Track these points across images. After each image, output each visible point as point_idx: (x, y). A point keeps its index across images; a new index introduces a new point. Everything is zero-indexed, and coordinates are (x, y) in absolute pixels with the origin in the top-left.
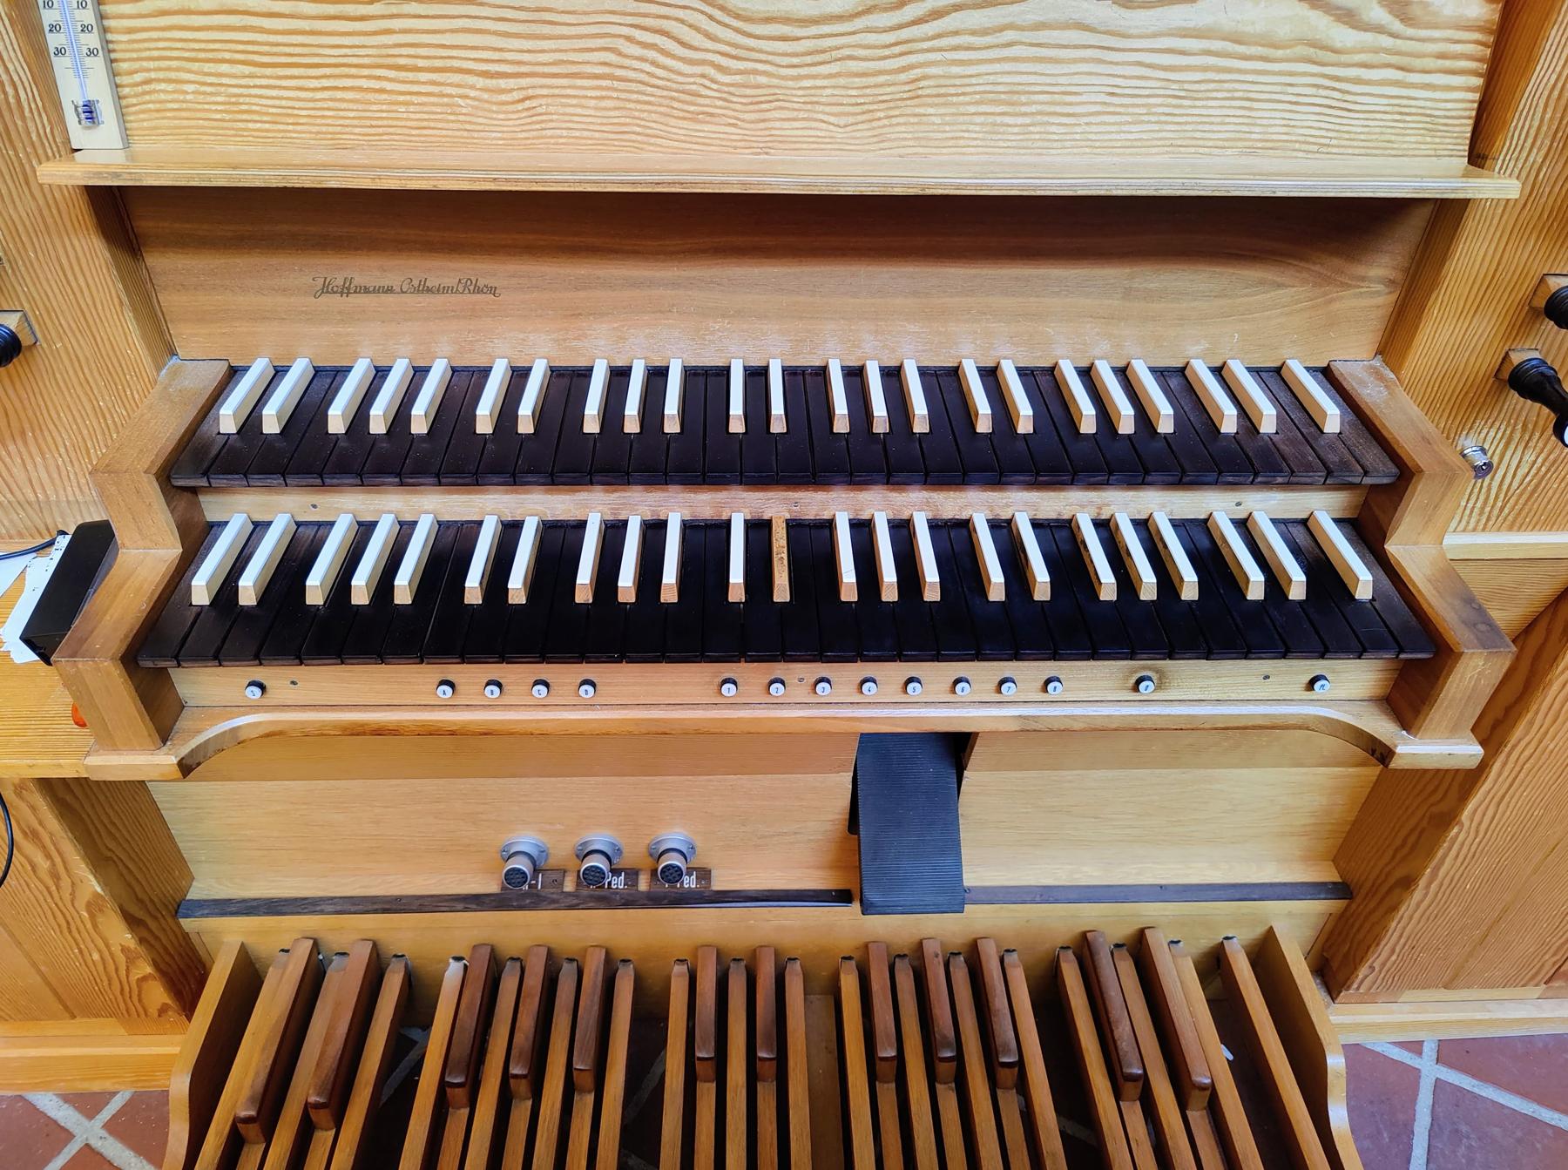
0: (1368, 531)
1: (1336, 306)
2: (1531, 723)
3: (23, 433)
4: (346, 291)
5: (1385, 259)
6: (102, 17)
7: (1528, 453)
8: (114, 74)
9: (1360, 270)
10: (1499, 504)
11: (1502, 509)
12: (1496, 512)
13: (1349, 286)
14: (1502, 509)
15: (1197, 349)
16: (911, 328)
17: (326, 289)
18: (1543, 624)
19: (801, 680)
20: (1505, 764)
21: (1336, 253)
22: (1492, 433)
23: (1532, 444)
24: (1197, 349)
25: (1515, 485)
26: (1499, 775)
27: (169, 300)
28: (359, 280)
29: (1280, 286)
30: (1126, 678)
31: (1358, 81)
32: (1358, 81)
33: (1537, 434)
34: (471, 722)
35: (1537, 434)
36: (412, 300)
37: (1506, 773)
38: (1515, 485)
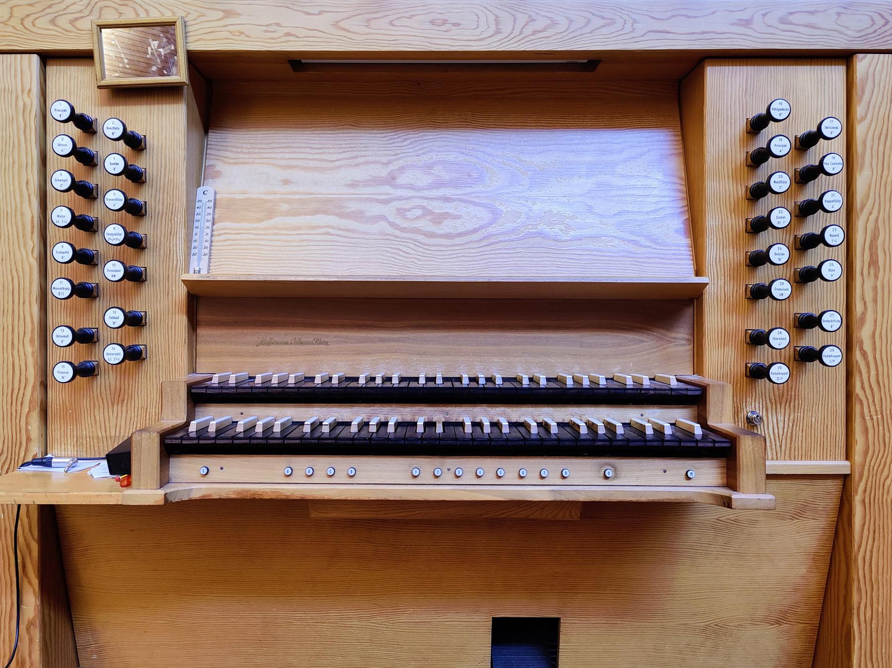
0: (702, 420)
1: (669, 350)
2: (859, 589)
3: (123, 401)
4: (269, 344)
5: (682, 330)
6: (211, 246)
7: (779, 415)
8: (210, 262)
9: (674, 335)
10: (778, 444)
11: (781, 447)
12: (778, 448)
13: (671, 342)
14: (781, 447)
15: (616, 369)
16: (496, 360)
17: (262, 343)
18: (840, 528)
19: (449, 470)
20: (859, 625)
21: (661, 327)
22: (757, 405)
23: (778, 410)
24: (616, 369)
25: (781, 433)
26: (860, 633)
27: (201, 348)
28: (276, 339)
29: (642, 341)
30: (599, 471)
31: (645, 263)
32: (645, 263)
33: (778, 406)
34: (297, 490)
35: (778, 406)
36: (294, 348)
37: (864, 632)
38: (781, 433)
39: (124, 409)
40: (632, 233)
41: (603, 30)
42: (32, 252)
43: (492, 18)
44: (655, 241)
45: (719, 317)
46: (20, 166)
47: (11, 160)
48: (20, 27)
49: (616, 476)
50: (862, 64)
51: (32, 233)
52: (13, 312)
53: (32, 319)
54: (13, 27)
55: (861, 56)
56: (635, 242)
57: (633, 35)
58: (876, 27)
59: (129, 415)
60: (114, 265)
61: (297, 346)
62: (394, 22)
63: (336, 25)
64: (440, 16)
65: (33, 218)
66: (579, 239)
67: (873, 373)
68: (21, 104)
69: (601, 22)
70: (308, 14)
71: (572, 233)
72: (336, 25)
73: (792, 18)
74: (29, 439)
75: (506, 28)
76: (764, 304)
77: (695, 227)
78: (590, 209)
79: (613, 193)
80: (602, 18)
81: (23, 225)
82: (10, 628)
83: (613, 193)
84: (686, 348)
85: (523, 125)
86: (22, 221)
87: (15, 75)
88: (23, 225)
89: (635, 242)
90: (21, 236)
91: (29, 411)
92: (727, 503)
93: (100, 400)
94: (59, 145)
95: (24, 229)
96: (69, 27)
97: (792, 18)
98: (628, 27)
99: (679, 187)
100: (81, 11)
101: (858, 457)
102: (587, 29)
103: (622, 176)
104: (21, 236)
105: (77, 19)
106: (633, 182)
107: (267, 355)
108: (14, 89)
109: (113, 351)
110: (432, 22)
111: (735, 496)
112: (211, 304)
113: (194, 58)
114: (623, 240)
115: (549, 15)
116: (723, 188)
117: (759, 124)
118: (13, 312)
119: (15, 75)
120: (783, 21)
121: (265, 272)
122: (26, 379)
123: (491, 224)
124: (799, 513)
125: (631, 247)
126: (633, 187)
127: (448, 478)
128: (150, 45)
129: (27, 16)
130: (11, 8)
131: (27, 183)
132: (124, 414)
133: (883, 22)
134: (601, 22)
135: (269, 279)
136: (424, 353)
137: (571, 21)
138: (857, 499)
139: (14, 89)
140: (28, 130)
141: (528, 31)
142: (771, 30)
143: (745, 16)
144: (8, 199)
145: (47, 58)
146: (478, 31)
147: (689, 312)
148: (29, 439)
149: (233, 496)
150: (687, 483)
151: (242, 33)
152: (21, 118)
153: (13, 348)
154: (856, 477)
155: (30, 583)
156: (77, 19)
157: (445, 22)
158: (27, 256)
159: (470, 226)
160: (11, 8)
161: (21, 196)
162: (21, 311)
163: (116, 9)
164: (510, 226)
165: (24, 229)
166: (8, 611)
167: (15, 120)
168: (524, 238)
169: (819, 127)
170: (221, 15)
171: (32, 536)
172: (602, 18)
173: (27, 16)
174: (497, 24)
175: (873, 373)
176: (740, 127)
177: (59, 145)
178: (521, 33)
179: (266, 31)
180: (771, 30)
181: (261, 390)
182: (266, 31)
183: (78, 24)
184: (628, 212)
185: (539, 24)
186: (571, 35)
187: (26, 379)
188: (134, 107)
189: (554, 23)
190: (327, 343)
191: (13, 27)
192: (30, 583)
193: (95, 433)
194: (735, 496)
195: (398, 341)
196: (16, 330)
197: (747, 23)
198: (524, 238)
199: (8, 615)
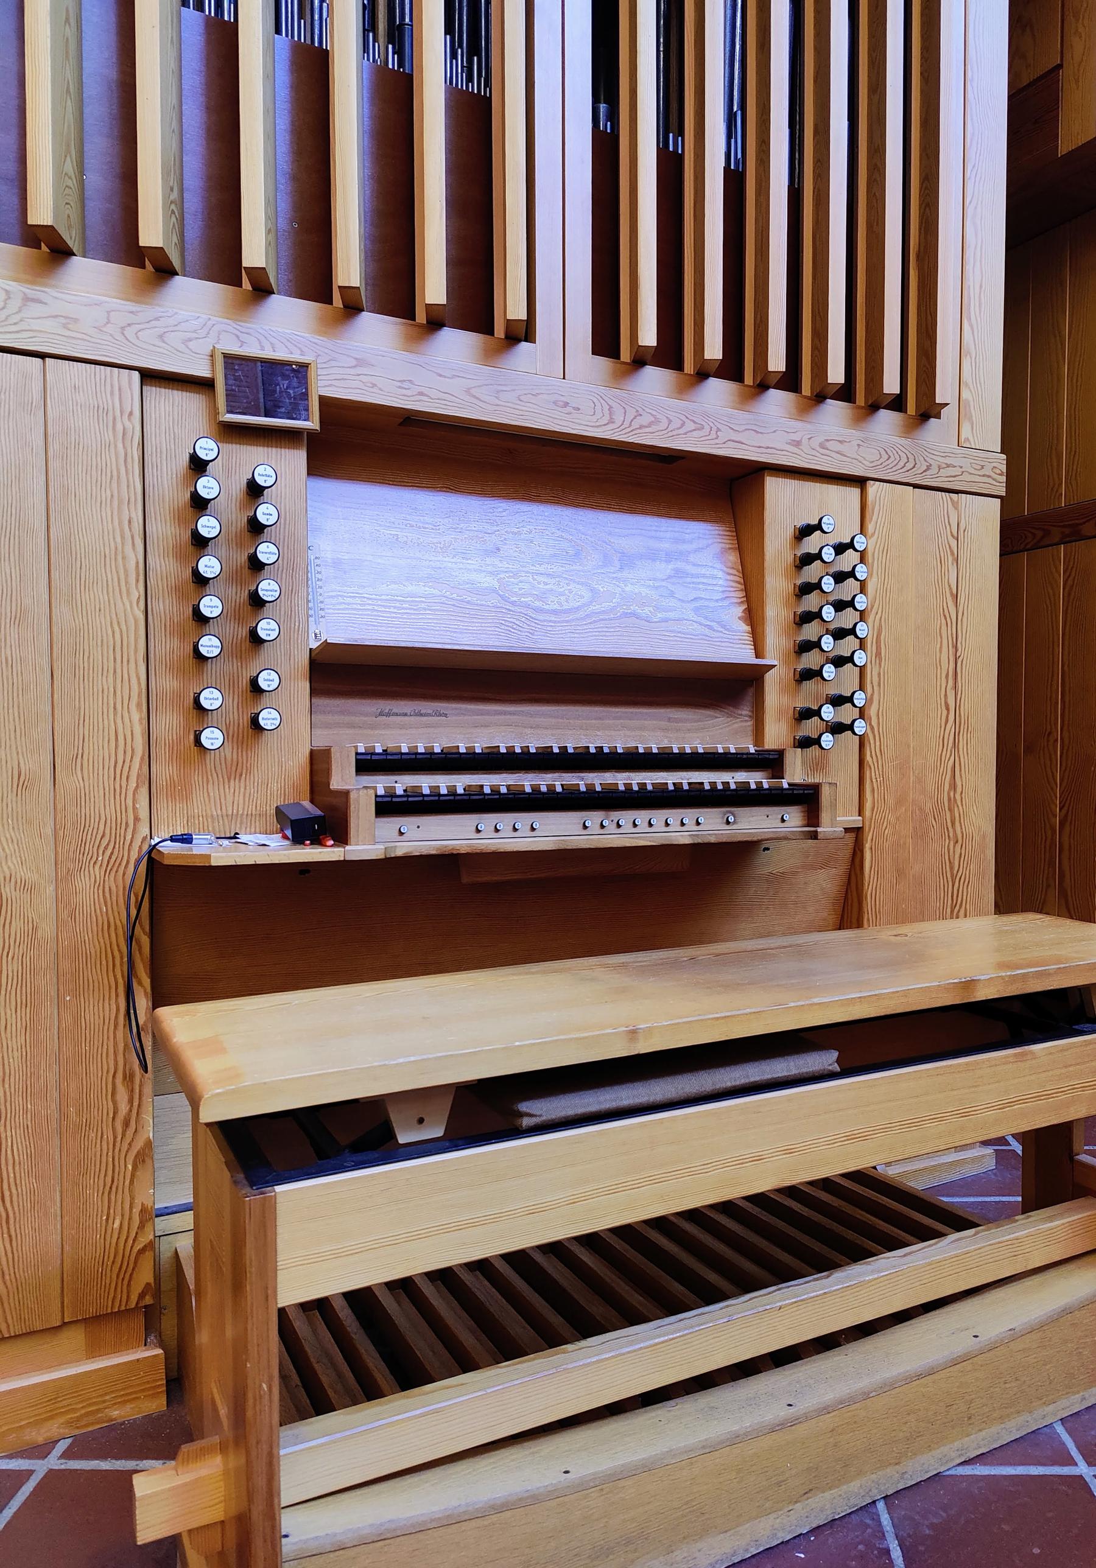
3: (241, 775)
4: (388, 715)
9: (740, 712)
17: (381, 714)
39: (242, 785)
40: (706, 618)
41: (695, 434)
42: (138, 602)
43: (606, 407)
44: (723, 626)
45: (776, 695)
46: (120, 502)
47: (109, 493)
48: (120, 337)
49: (735, 822)
50: (872, 488)
51: (137, 581)
52: (115, 672)
53: (139, 679)
54: (111, 335)
55: (872, 482)
56: (710, 627)
57: (717, 441)
58: (882, 460)
59: (248, 791)
60: (269, 623)
61: (418, 718)
62: (522, 398)
63: (468, 391)
64: (563, 399)
65: (137, 563)
66: (666, 620)
67: (878, 744)
68: (119, 427)
69: (692, 426)
70: (440, 375)
71: (659, 615)
72: (468, 391)
73: (828, 444)
74: (137, 819)
75: (619, 418)
76: (809, 685)
77: (753, 617)
78: (672, 594)
79: (689, 580)
80: (694, 422)
81: (126, 571)
82: (115, 1037)
83: (689, 580)
84: (750, 723)
85: (609, 508)
86: (124, 566)
87: (112, 393)
88: (126, 571)
89: (710, 627)
90: (123, 584)
91: (137, 786)
92: (814, 836)
93: (215, 775)
94: (204, 487)
95: (127, 576)
96: (182, 347)
97: (828, 444)
98: (713, 432)
99: (738, 579)
100: (195, 331)
101: (868, 812)
102: (681, 431)
103: (694, 565)
104: (123, 584)
105: (190, 340)
106: (703, 571)
107: (387, 726)
108: (110, 408)
109: (270, 716)
110: (555, 403)
111: (819, 830)
112: (344, 673)
113: (324, 401)
114: (701, 624)
115: (654, 413)
116: (777, 585)
117: (806, 531)
118: (115, 672)
119: (112, 393)
120: (822, 446)
121: (416, 639)
122: (133, 750)
123: (591, 602)
124: (824, 865)
125: (707, 631)
126: (704, 576)
127: (610, 827)
128: (278, 384)
129: (129, 325)
130: (108, 312)
131: (130, 522)
132: (242, 790)
133: (886, 457)
134: (692, 426)
135: (417, 645)
136: (538, 727)
137: (670, 421)
138: (867, 846)
139: (110, 408)
140: (129, 460)
141: (635, 425)
142: (814, 453)
143: (796, 437)
144: (106, 538)
145: (150, 377)
146: (594, 418)
147: (751, 692)
148: (137, 819)
149: (434, 852)
150: (782, 825)
151: (374, 385)
152: (120, 445)
153: (115, 714)
154: (867, 829)
155: (140, 983)
156: (190, 340)
157: (566, 404)
158: (131, 607)
159: (573, 604)
160: (108, 312)
161: (123, 537)
162: (125, 672)
163: (238, 337)
164: (606, 605)
165: (127, 576)
166: (113, 1018)
167: (112, 446)
168: (620, 617)
169: (853, 539)
170: (354, 363)
171: (143, 930)
172: (694, 422)
173: (129, 325)
174: (610, 414)
175: (878, 744)
176: (790, 532)
177: (204, 487)
178: (630, 425)
179: (400, 387)
180: (814, 453)
181: (408, 757)
182: (400, 387)
183: (191, 344)
184: (702, 599)
185: (645, 419)
186: (670, 434)
187: (133, 750)
188: (249, 448)
189: (656, 421)
190: (446, 715)
191: (111, 335)
192: (140, 983)
193: (209, 812)
194: (819, 830)
195: (510, 714)
196: (119, 693)
197: (797, 444)
198: (620, 617)
199: (112, 1022)
